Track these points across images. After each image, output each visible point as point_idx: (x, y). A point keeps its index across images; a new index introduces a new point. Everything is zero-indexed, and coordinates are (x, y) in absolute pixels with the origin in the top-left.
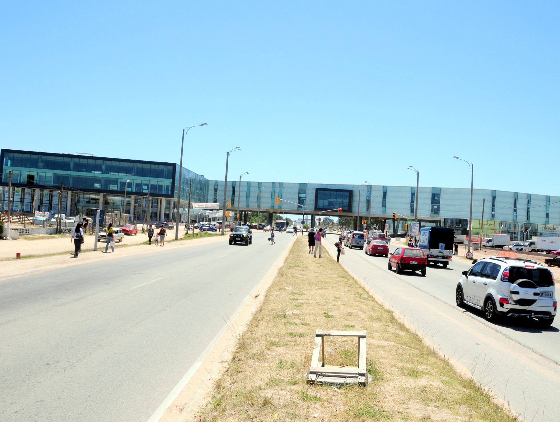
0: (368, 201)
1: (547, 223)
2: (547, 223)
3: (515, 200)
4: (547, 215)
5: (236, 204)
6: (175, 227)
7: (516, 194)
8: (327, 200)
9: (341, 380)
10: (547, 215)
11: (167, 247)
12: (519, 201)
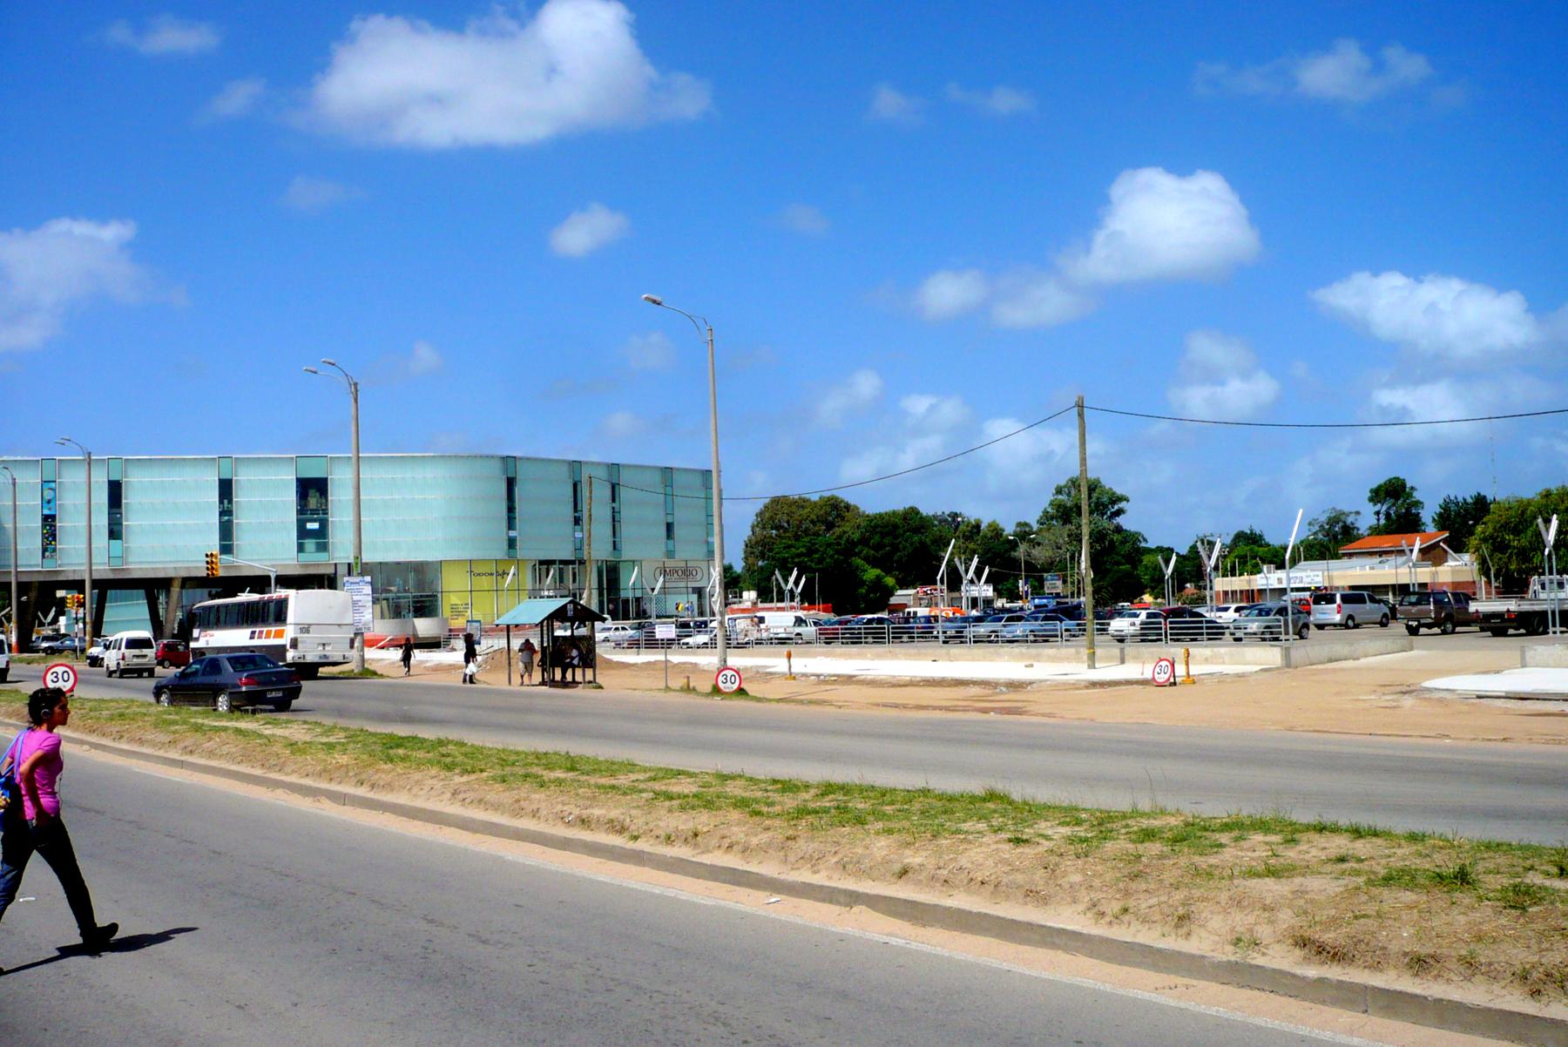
0: (49, 520)
1: (670, 554)
2: (670, 554)
7: (575, 466)
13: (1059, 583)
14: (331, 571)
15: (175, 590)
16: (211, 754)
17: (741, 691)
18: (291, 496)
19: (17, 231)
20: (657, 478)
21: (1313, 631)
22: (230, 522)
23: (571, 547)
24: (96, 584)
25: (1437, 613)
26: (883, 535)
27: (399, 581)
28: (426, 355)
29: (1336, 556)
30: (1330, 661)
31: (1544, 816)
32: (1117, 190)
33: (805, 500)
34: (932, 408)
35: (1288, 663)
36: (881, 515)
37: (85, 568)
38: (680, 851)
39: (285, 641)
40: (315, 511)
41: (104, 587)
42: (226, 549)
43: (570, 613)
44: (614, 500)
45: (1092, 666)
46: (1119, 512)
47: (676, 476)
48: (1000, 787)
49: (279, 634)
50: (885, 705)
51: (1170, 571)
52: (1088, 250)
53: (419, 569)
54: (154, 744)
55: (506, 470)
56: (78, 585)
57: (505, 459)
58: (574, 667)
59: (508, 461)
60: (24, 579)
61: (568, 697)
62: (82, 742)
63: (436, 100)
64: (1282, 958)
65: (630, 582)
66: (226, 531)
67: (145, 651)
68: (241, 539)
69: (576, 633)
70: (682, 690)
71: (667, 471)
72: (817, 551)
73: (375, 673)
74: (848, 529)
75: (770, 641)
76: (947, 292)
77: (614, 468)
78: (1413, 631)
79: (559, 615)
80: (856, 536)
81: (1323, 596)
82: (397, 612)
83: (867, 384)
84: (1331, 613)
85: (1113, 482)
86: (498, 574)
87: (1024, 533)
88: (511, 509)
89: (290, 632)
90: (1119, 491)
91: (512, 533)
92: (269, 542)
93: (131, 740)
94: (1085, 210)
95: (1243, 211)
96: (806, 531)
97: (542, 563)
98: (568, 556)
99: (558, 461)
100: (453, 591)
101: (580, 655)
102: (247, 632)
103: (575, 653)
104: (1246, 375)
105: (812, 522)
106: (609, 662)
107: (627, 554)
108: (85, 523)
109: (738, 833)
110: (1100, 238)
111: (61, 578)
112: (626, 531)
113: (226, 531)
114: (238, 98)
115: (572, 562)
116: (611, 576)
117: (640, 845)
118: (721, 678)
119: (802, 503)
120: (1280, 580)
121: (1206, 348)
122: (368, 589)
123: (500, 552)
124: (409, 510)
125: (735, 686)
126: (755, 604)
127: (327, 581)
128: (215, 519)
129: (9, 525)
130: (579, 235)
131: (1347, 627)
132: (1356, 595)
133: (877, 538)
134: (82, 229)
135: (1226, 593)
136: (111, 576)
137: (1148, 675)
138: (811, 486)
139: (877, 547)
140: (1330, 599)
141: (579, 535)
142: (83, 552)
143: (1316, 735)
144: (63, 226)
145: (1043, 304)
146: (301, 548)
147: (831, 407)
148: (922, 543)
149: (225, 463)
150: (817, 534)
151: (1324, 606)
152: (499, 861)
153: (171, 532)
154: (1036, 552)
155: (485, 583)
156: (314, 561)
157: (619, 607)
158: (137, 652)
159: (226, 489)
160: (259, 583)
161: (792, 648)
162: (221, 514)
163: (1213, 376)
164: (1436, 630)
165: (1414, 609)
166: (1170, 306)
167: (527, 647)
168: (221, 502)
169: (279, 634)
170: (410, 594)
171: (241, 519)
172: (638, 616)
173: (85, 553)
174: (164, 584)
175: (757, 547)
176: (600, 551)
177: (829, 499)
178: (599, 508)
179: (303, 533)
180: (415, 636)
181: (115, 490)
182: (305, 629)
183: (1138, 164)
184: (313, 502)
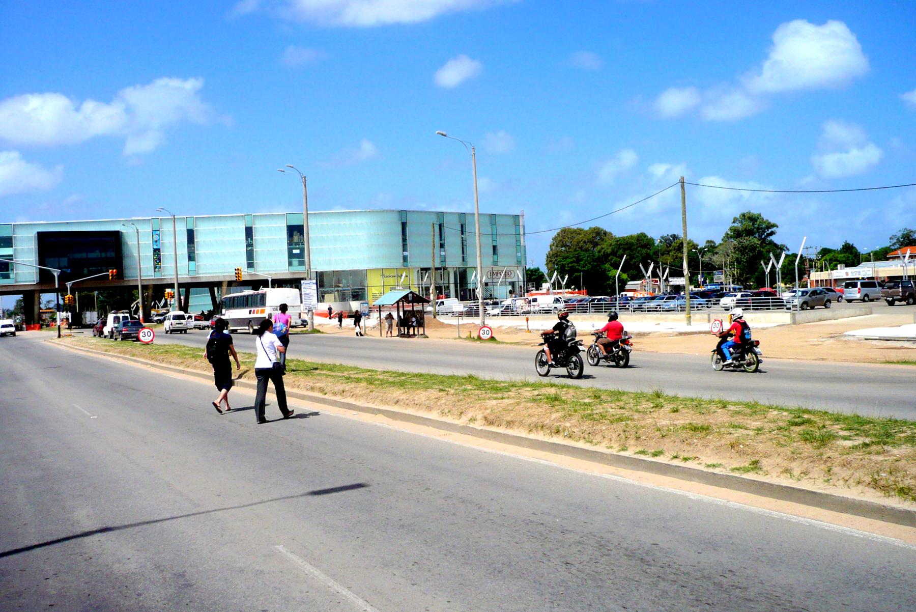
0: (157, 251)
1: (495, 263)
2: (495, 263)
4: (495, 248)
7: (440, 214)
10: (495, 248)
13: (723, 277)
15: (225, 287)
16: (195, 367)
17: (492, 338)
19: (138, 86)
21: (844, 303)
22: (252, 250)
24: (181, 285)
25: (904, 292)
27: (344, 281)
28: (368, 148)
29: (887, 259)
30: (820, 320)
32: (777, 36)
33: (581, 230)
34: (668, 171)
35: (794, 322)
37: (175, 277)
38: (338, 398)
40: (297, 244)
41: (188, 287)
42: (250, 265)
43: (410, 299)
45: (689, 324)
46: (772, 233)
48: (473, 373)
49: (263, 312)
50: (898, 362)
51: (768, 270)
52: (760, 74)
53: (354, 273)
54: (175, 364)
55: (401, 217)
56: (171, 286)
58: (414, 327)
59: (402, 213)
60: (145, 283)
61: (403, 342)
62: (147, 364)
64: (479, 425)
66: (250, 255)
67: (182, 321)
68: (258, 260)
69: (415, 309)
70: (467, 338)
71: (493, 217)
72: (582, 260)
73: (319, 332)
74: (606, 247)
75: (540, 312)
76: (674, 101)
77: (462, 215)
78: (891, 304)
79: (405, 298)
80: (609, 251)
81: (851, 283)
82: (343, 298)
83: (628, 158)
84: (855, 293)
85: (768, 216)
86: (398, 276)
87: (712, 247)
88: (404, 240)
90: (772, 221)
91: (405, 253)
92: (273, 260)
93: (167, 362)
94: (758, 48)
95: (859, 46)
96: (581, 248)
97: (422, 269)
100: (374, 286)
101: (417, 320)
102: (247, 310)
103: (414, 319)
104: (861, 146)
105: (585, 242)
106: (442, 325)
107: (470, 264)
108: (173, 253)
109: (358, 391)
110: (767, 65)
111: (165, 282)
113: (250, 255)
115: (440, 269)
116: (462, 276)
117: (326, 397)
119: (579, 232)
120: (847, 274)
121: (836, 130)
122: (315, 287)
123: (399, 263)
124: (347, 243)
125: (489, 336)
126: (548, 290)
127: (295, 283)
129: (136, 254)
130: (453, 74)
131: (864, 301)
132: (869, 283)
134: (175, 83)
135: (817, 281)
136: (190, 281)
138: (581, 219)
140: (855, 286)
141: (443, 253)
142: (176, 268)
143: (866, 365)
145: (732, 107)
146: (290, 264)
147: (607, 172)
149: (249, 218)
150: (587, 250)
151: (851, 289)
153: (221, 258)
154: (715, 258)
155: (392, 281)
156: (297, 270)
157: (465, 293)
158: (178, 321)
159: (249, 232)
160: (265, 283)
161: (528, 316)
163: (840, 147)
164: (904, 303)
165: (890, 291)
166: (812, 106)
167: (390, 317)
168: (247, 239)
169: (263, 312)
170: (345, 287)
171: (258, 249)
172: (474, 299)
174: (219, 284)
175: (552, 259)
176: (454, 262)
177: (595, 229)
178: (452, 239)
179: (291, 256)
180: (351, 311)
181: (191, 235)
183: (790, 18)
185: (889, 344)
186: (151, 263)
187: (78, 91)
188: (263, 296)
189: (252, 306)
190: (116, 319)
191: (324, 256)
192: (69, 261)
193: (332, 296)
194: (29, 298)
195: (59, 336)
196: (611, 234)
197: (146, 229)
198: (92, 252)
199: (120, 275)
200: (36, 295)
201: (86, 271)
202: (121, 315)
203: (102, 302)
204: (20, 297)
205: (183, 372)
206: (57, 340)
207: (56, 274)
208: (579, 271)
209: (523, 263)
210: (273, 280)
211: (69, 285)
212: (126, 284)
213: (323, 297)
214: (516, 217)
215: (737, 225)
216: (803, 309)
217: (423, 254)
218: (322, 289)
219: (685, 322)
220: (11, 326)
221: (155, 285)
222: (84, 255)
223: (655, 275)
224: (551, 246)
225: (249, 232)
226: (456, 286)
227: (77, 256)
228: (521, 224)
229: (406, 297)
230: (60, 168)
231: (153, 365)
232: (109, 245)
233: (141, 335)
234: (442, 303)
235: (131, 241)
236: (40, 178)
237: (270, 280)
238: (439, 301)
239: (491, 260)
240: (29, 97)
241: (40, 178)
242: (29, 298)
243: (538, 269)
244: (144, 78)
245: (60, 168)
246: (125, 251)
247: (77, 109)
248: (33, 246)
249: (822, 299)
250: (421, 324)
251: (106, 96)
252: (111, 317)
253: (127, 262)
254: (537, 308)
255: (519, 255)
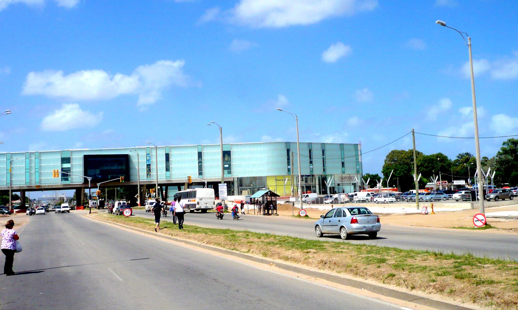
0: (149, 166)
1: (343, 172)
2: (343, 172)
3: (310, 151)
4: (343, 163)
5: (153, 173)
6: (419, 211)
7: (310, 144)
8: (98, 168)
9: (288, 263)
10: (343, 163)
11: (272, 216)
12: (314, 153)
14: (232, 180)
17: (306, 216)
18: (220, 156)
20: (338, 147)
22: (201, 165)
23: (309, 171)
24: (161, 185)
26: (428, 163)
28: (283, 100)
31: (509, 252)
33: (403, 151)
35: (473, 208)
36: (428, 156)
38: (176, 238)
39: (196, 203)
40: (227, 161)
42: (200, 174)
44: (323, 155)
45: (418, 209)
47: (345, 147)
49: (195, 201)
50: (459, 228)
53: (261, 178)
55: (287, 146)
57: (286, 143)
59: (287, 144)
60: (142, 184)
63: (279, 10)
65: (329, 183)
66: (200, 168)
68: (205, 171)
71: (342, 145)
72: (398, 170)
77: (323, 145)
83: (446, 104)
88: (288, 159)
89: (197, 200)
91: (289, 167)
98: (308, 174)
99: (303, 143)
101: (273, 206)
102: (187, 200)
103: (271, 205)
105: (406, 159)
107: (328, 172)
112: (327, 165)
113: (200, 168)
114: (211, 15)
115: (310, 176)
116: (323, 180)
118: (301, 212)
119: (402, 152)
122: (226, 187)
123: (285, 173)
124: (255, 161)
128: (197, 164)
129: (137, 168)
130: (333, 54)
133: (426, 164)
134: (168, 63)
136: (167, 183)
137: (420, 212)
139: (426, 167)
141: (311, 167)
142: (160, 176)
144: (161, 63)
147: (432, 113)
148: (443, 166)
149: (200, 147)
152: (155, 240)
153: (183, 169)
159: (200, 155)
162: (199, 163)
168: (199, 159)
169: (195, 201)
171: (205, 164)
173: (156, 175)
174: (183, 184)
176: (318, 172)
179: (224, 168)
181: (167, 156)
182: (201, 199)
184: (226, 159)
185: (497, 220)
186: (145, 173)
187: (111, 69)
188: (195, 192)
189: (190, 198)
190: (119, 204)
191: (241, 170)
192: (101, 171)
193: (247, 191)
194: (79, 190)
195: (90, 213)
196: (422, 153)
197: (143, 153)
198: (113, 166)
199: (128, 178)
200: (82, 190)
201: (109, 177)
202: (122, 202)
203: (121, 193)
204: (75, 190)
205: (133, 229)
206: (88, 215)
207: (89, 180)
208: (396, 177)
209: (360, 172)
210: (208, 182)
211: (98, 184)
212: (131, 184)
213: (241, 192)
214: (356, 146)
215: (505, 146)
216: (496, 201)
217: (301, 168)
218: (241, 188)
219: (416, 208)
220: (67, 207)
221: (147, 185)
222: (109, 168)
223: (438, 180)
224: (385, 161)
225: (200, 155)
226: (319, 186)
227: (105, 168)
228: (359, 149)
229: (267, 193)
230: (101, 113)
231: (123, 227)
232: (123, 162)
233: (125, 212)
234: (308, 196)
235: (134, 160)
236: (91, 120)
237: (206, 183)
238: (306, 195)
239: (341, 170)
240: (83, 71)
241: (91, 120)
242: (79, 190)
243: (378, 175)
244: (151, 61)
245: (101, 113)
246: (131, 165)
247: (111, 79)
248: (81, 162)
249: (508, 195)
250: (275, 208)
251: (128, 72)
252: (116, 203)
253: (132, 172)
254: (357, 199)
255: (358, 167)
